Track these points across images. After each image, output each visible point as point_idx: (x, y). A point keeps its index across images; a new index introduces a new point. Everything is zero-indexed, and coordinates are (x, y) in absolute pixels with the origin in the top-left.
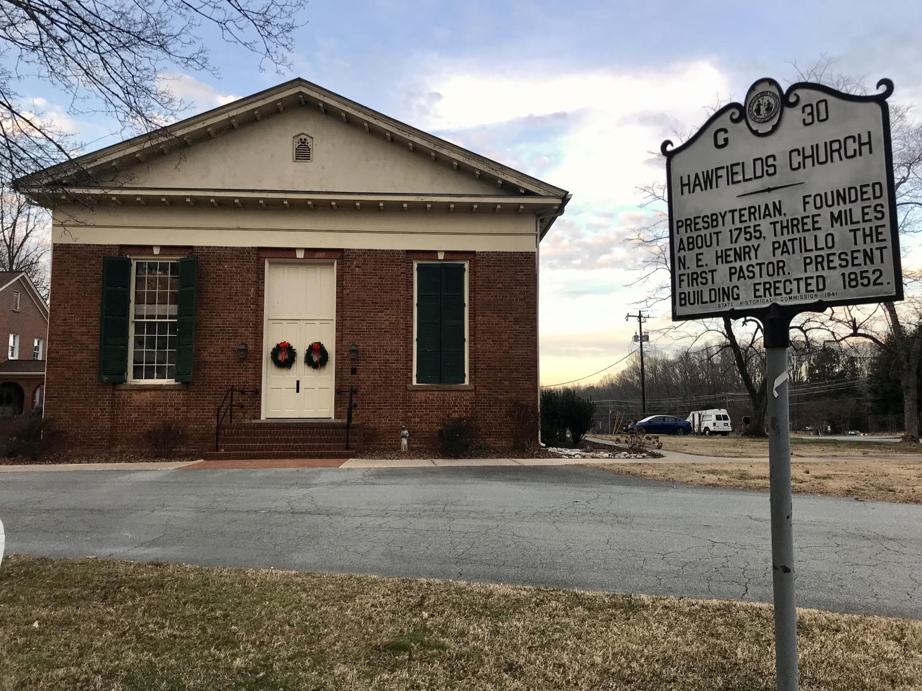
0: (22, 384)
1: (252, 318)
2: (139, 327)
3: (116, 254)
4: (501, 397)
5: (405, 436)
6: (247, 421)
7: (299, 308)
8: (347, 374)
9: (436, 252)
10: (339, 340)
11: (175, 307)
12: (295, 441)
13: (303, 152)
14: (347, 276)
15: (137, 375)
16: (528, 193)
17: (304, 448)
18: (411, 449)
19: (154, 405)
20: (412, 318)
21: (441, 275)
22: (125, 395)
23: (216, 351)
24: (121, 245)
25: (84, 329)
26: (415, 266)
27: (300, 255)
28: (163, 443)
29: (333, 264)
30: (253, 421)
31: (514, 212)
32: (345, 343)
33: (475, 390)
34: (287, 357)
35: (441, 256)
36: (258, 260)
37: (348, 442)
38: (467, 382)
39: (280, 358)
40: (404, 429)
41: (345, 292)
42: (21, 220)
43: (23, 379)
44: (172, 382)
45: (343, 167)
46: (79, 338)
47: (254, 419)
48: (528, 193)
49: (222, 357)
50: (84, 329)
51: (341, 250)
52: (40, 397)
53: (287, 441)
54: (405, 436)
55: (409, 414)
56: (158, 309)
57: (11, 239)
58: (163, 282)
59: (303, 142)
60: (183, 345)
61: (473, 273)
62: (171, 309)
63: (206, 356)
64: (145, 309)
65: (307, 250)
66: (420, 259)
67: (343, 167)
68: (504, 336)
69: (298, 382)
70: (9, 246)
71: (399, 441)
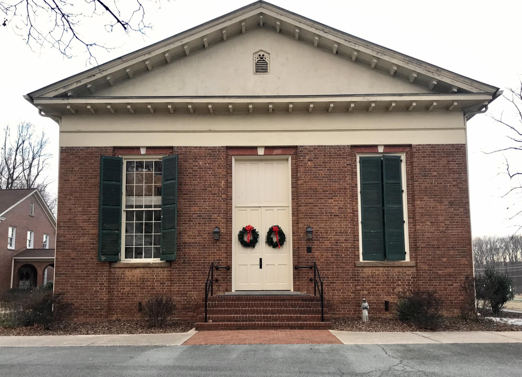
0: (36, 265)
1: (223, 206)
2: (130, 216)
3: (110, 153)
4: (440, 272)
5: (366, 308)
6: (221, 294)
7: (262, 196)
8: (303, 252)
9: (376, 146)
10: (296, 222)
11: (160, 198)
12: (273, 312)
13: (261, 66)
14: (301, 169)
15: (128, 255)
16: (461, 91)
17: (282, 319)
18: (371, 319)
19: (143, 280)
20: (357, 203)
21: (381, 168)
22: (118, 272)
23: (193, 234)
24: (114, 147)
25: (85, 217)
26: (358, 160)
27: (261, 152)
28: (158, 315)
29: (287, 160)
30: (226, 293)
31: (446, 109)
32: (301, 225)
33: (416, 266)
34: (251, 238)
35: (381, 150)
36: (227, 157)
37: (322, 315)
38: (408, 258)
39: (246, 239)
40: (365, 301)
41: (300, 182)
42: (35, 162)
43: (37, 262)
44: (158, 260)
45: (294, 75)
46: (81, 224)
47: (227, 291)
48: (461, 91)
49: (198, 239)
50: (85, 217)
51: (296, 147)
52: (47, 276)
53: (266, 312)
54: (366, 308)
55: (358, 288)
56: (145, 200)
57: (28, 176)
58: (149, 179)
59: (262, 58)
60: (164, 229)
61: (410, 164)
62: (155, 200)
63: (186, 239)
64: (134, 200)
65: (266, 148)
66: (362, 153)
67: (294, 75)
68: (440, 218)
69: (261, 259)
70: (27, 181)
71: (360, 312)
